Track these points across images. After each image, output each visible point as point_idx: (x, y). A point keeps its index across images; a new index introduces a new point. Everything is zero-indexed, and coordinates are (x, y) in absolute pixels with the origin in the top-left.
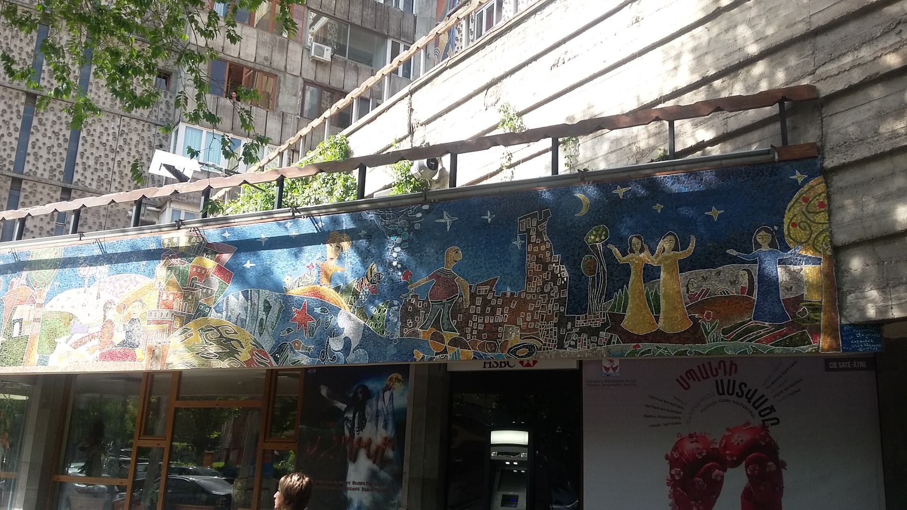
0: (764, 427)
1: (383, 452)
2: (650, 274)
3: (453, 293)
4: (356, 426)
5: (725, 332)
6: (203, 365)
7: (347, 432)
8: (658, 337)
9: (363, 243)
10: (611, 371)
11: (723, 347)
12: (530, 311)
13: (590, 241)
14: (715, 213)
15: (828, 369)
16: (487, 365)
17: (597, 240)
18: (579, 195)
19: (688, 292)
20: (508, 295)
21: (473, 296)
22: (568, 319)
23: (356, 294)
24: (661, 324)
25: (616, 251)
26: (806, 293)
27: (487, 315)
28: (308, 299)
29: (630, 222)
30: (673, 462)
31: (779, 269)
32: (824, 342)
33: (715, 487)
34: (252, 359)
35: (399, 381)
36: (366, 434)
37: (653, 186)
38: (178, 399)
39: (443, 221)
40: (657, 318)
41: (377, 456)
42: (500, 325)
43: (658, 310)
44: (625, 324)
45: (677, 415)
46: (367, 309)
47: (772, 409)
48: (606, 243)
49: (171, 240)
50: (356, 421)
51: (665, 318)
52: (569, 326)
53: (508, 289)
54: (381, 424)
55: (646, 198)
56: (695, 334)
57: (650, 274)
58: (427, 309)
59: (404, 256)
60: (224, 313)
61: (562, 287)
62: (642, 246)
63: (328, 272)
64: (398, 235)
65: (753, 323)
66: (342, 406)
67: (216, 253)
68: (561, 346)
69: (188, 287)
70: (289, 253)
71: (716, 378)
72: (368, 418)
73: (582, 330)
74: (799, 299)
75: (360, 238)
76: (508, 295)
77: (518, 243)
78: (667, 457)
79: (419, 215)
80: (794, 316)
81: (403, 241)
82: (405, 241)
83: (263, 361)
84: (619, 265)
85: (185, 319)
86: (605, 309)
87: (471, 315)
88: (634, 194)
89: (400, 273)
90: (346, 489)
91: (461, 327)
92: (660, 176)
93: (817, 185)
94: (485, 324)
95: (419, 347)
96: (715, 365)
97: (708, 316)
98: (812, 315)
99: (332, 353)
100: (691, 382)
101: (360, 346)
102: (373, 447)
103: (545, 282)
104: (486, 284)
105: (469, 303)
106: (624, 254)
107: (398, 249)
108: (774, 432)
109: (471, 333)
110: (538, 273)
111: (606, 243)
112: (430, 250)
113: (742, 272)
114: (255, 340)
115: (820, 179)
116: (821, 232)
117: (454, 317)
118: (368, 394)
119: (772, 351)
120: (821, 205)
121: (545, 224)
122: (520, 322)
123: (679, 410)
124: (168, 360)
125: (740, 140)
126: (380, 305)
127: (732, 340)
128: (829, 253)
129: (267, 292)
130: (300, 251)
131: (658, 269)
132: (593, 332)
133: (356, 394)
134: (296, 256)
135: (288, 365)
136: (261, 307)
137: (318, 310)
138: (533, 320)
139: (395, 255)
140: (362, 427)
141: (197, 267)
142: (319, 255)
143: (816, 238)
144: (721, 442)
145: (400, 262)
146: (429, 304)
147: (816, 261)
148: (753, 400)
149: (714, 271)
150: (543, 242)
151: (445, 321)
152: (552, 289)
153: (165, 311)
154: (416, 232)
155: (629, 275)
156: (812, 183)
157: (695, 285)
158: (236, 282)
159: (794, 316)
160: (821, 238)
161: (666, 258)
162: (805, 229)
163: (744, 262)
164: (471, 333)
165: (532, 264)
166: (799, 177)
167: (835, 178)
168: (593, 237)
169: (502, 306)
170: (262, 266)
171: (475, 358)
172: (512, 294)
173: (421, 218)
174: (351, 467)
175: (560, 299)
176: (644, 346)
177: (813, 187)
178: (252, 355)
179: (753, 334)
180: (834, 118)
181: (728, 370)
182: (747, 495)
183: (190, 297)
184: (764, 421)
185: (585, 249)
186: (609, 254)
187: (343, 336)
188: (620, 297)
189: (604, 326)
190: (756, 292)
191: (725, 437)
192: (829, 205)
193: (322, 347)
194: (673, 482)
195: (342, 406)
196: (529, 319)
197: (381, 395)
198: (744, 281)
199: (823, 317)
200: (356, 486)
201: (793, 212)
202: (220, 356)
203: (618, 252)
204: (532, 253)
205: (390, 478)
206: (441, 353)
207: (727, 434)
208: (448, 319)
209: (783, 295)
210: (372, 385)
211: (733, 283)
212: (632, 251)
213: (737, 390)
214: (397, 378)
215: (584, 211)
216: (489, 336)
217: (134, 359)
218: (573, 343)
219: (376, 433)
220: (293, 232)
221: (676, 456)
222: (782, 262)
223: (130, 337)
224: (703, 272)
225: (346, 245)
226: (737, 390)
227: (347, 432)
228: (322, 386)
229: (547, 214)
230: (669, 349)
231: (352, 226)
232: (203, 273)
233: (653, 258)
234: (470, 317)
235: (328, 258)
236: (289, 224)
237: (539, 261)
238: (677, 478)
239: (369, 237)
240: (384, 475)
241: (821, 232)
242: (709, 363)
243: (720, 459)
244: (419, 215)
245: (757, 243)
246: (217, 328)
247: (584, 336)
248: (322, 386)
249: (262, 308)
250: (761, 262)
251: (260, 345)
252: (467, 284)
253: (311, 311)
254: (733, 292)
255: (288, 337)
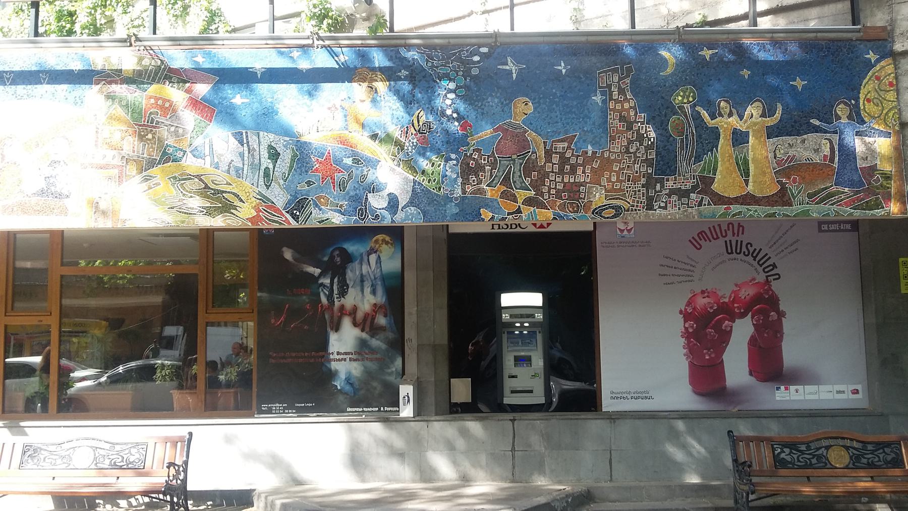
0: (767, 282)
1: (373, 318)
2: (739, 138)
3: (524, 148)
4: (336, 292)
5: (810, 196)
6: (183, 222)
7: (324, 300)
8: (748, 199)
9: (406, 87)
10: (626, 232)
11: (808, 210)
12: (615, 171)
13: (677, 102)
14: (799, 83)
15: (820, 230)
16: (496, 227)
17: (685, 101)
18: (664, 53)
19: (775, 158)
20: (590, 154)
21: (548, 154)
22: (657, 181)
23: (400, 145)
24: (750, 188)
25: (705, 114)
26: (879, 163)
27: (566, 173)
28: (332, 146)
29: (717, 86)
30: (687, 317)
31: (856, 141)
32: (894, 208)
33: (725, 337)
34: (258, 216)
35: (387, 243)
36: (349, 300)
37: (740, 51)
38: (62, 264)
39: (507, 68)
40: (747, 182)
41: (366, 324)
42: (581, 184)
43: (747, 174)
44: (715, 187)
45: (690, 273)
46: (416, 162)
47: (774, 266)
48: (695, 105)
49: (107, 59)
50: (335, 287)
51: (754, 182)
52: (658, 187)
53: (590, 147)
54: (368, 290)
55: (733, 63)
56: (782, 198)
57: (739, 138)
58: (493, 165)
59: (462, 107)
60: (208, 159)
61: (648, 148)
62: (731, 111)
63: (359, 116)
64: (450, 80)
65: (834, 189)
66: (317, 271)
67: (185, 82)
68: (650, 207)
69: (144, 125)
70: (300, 90)
71: (726, 239)
72: (351, 284)
73: (672, 192)
74: (873, 169)
75: (400, 79)
76: (590, 154)
77: (598, 98)
78: (681, 312)
79: (476, 58)
80: (869, 184)
81: (458, 87)
82: (461, 87)
83: (276, 219)
84: (707, 128)
85: (146, 165)
86: (695, 171)
87: (548, 173)
88: (721, 60)
89: (456, 124)
90: (330, 361)
91: (537, 186)
92: (747, 41)
93: (886, 67)
94: (565, 184)
95: (487, 206)
96: (724, 227)
97: (794, 182)
98: (885, 183)
99: (373, 211)
100: (702, 242)
101: (411, 203)
102: (360, 315)
103: (630, 142)
104: (562, 141)
105: (544, 160)
106: (713, 117)
107: (452, 96)
108: (775, 286)
109: (549, 192)
110: (622, 132)
111: (695, 105)
112: (493, 102)
113: (824, 141)
114: (260, 193)
115: (889, 60)
116: (890, 110)
117: (527, 174)
118: (348, 258)
119: (851, 214)
120: (891, 84)
121: (628, 81)
122: (604, 182)
123: (692, 268)
124: (123, 216)
125: (794, 15)
126: (434, 158)
127: (817, 203)
128: (897, 128)
129: (272, 136)
130: (316, 89)
131: (747, 134)
132: (683, 194)
133: (332, 257)
134: (310, 94)
135: (313, 223)
136: (265, 154)
137: (348, 161)
138: (618, 180)
139: (448, 102)
140: (343, 293)
141: (157, 99)
142: (344, 95)
143: (887, 114)
144: (730, 297)
145: (456, 111)
146: (496, 160)
147: (888, 135)
148: (758, 259)
149: (799, 139)
150: (626, 100)
151: (517, 178)
152: (638, 149)
153: (110, 153)
154: (475, 78)
155: (718, 138)
156: (883, 63)
157: (782, 152)
158: (223, 122)
159: (869, 184)
160: (891, 114)
161: (755, 124)
162: (878, 106)
163: (826, 132)
164: (549, 192)
165: (614, 122)
166: (872, 56)
167: (902, 61)
168: (680, 98)
169: (584, 165)
170: (261, 103)
171: (554, 218)
172: (594, 153)
173: (478, 62)
174: (333, 337)
175: (647, 159)
176: (735, 208)
177: (883, 67)
178: (258, 211)
179: (834, 199)
180: (903, 6)
181: (736, 232)
182: (753, 342)
183: (150, 136)
184: (767, 277)
185: (672, 110)
186: (697, 117)
187: (386, 192)
188: (709, 160)
189: (694, 189)
190: (837, 159)
191: (733, 292)
192: (897, 85)
193: (359, 204)
194: (687, 335)
195: (317, 271)
196: (614, 179)
197: (365, 258)
198: (826, 150)
199: (894, 187)
200: (342, 357)
201: (868, 88)
202: (209, 212)
203: (706, 115)
204: (614, 110)
205: (383, 346)
206: (513, 213)
207: (736, 289)
208: (520, 176)
209: (860, 164)
210: (351, 248)
211: (817, 151)
212: (721, 115)
213: (744, 249)
214: (384, 240)
215: (669, 70)
216: (569, 196)
217: (64, 212)
218: (663, 205)
219: (364, 299)
220: (304, 65)
221: (689, 310)
222: (858, 134)
223: (53, 185)
224: (789, 139)
225: (381, 86)
226: (744, 249)
227: (324, 300)
228: (285, 249)
229: (629, 70)
230: (759, 211)
231: (387, 64)
232: (168, 108)
233: (741, 123)
234: (547, 175)
235: (357, 101)
236: (296, 54)
237: (622, 119)
238: (691, 330)
239: (412, 79)
240: (375, 343)
241: (890, 110)
242: (719, 225)
243: (730, 311)
244: (476, 58)
245: (837, 115)
246: (199, 177)
247: (674, 198)
248: (285, 249)
249: (266, 155)
250: (841, 133)
251: (269, 199)
252: (540, 140)
253: (339, 162)
254: (817, 159)
255: (309, 191)
